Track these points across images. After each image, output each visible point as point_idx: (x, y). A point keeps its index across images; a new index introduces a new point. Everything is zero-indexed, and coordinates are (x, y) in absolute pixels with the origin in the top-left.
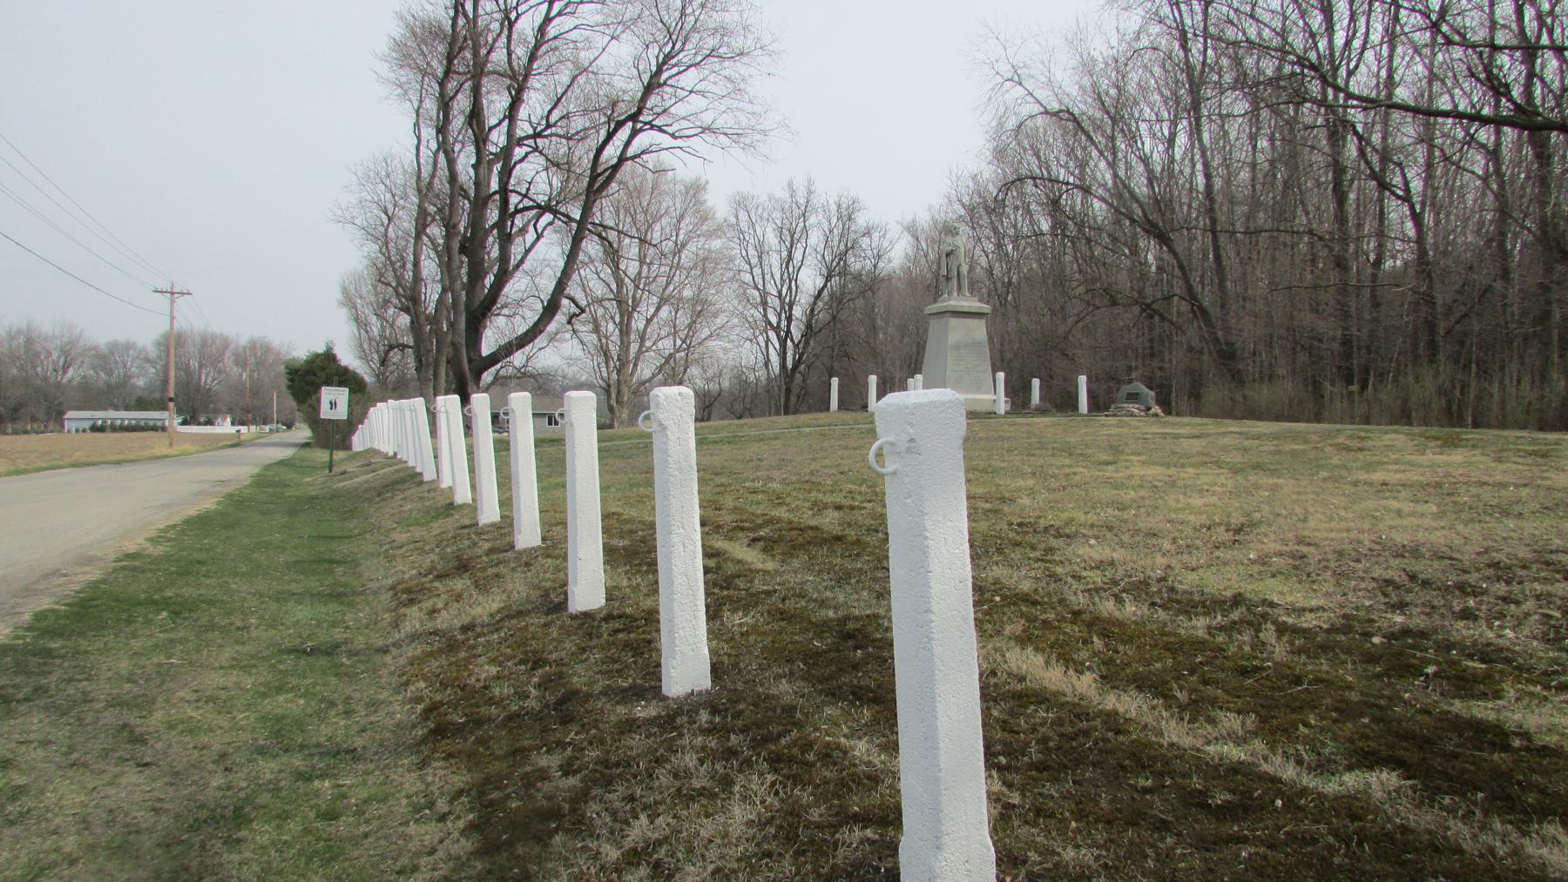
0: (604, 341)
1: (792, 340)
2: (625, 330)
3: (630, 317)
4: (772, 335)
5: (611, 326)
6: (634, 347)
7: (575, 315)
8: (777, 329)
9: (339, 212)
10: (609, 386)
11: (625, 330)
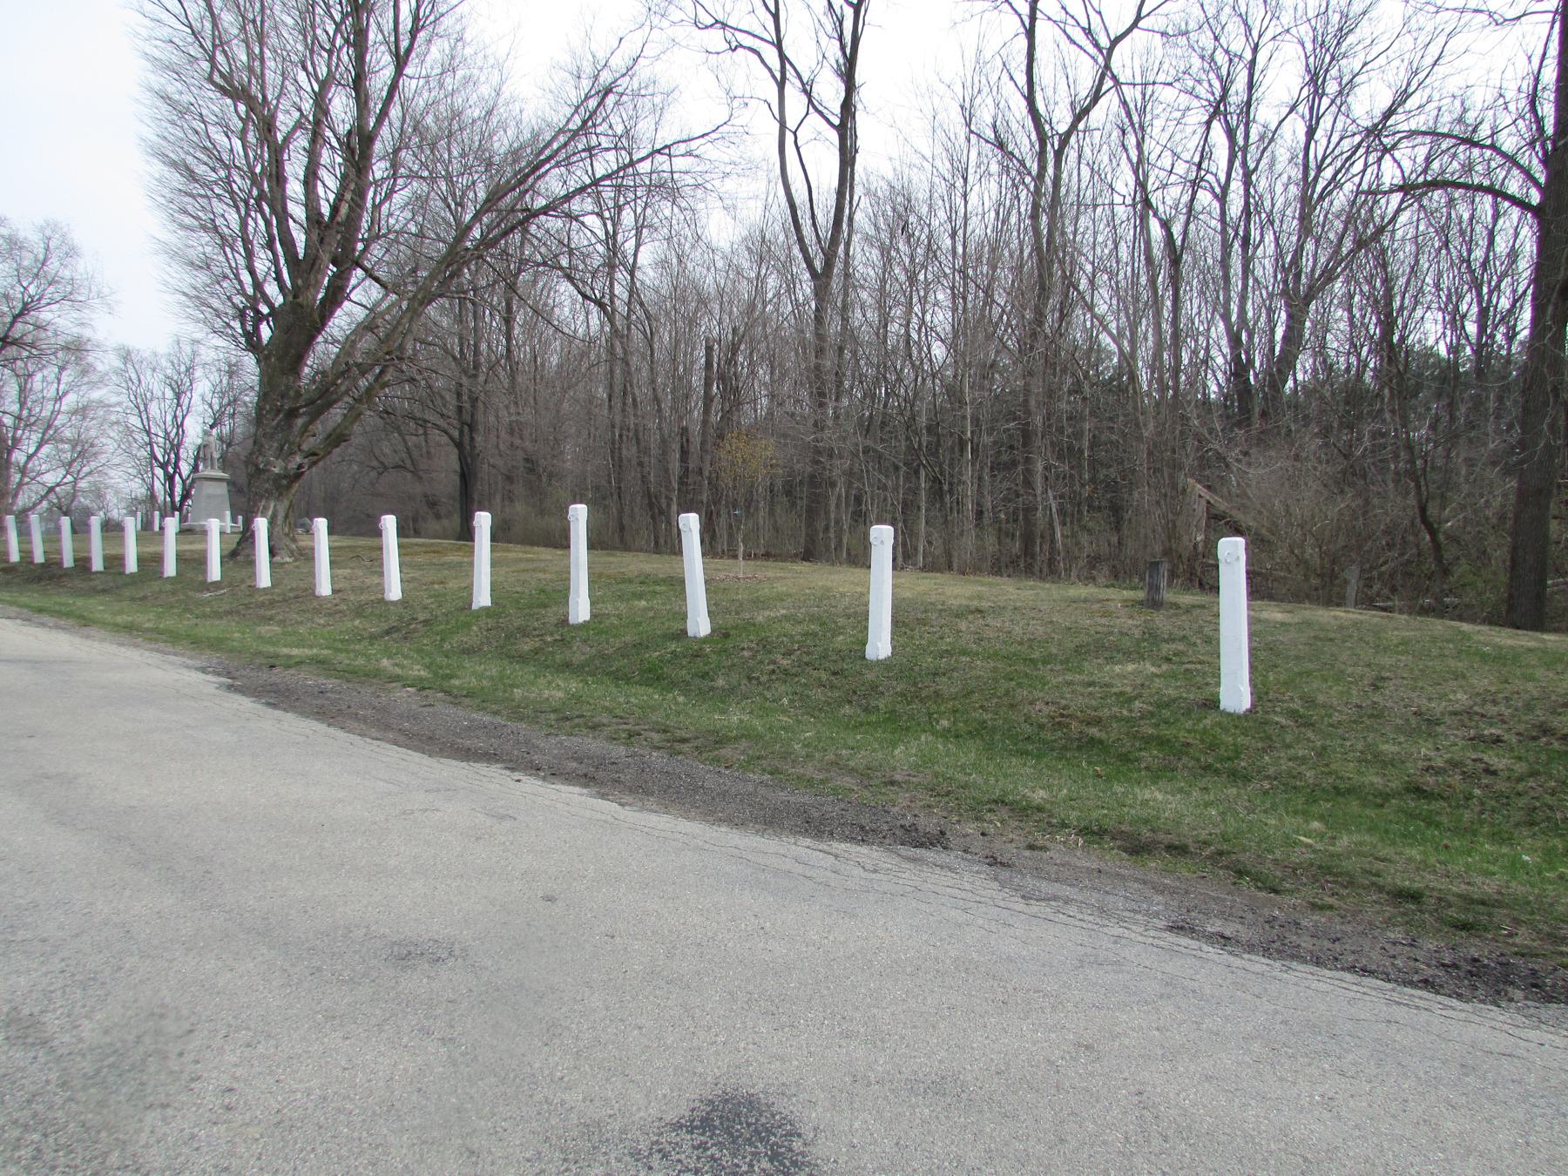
4: (159, 472)
8: (164, 466)
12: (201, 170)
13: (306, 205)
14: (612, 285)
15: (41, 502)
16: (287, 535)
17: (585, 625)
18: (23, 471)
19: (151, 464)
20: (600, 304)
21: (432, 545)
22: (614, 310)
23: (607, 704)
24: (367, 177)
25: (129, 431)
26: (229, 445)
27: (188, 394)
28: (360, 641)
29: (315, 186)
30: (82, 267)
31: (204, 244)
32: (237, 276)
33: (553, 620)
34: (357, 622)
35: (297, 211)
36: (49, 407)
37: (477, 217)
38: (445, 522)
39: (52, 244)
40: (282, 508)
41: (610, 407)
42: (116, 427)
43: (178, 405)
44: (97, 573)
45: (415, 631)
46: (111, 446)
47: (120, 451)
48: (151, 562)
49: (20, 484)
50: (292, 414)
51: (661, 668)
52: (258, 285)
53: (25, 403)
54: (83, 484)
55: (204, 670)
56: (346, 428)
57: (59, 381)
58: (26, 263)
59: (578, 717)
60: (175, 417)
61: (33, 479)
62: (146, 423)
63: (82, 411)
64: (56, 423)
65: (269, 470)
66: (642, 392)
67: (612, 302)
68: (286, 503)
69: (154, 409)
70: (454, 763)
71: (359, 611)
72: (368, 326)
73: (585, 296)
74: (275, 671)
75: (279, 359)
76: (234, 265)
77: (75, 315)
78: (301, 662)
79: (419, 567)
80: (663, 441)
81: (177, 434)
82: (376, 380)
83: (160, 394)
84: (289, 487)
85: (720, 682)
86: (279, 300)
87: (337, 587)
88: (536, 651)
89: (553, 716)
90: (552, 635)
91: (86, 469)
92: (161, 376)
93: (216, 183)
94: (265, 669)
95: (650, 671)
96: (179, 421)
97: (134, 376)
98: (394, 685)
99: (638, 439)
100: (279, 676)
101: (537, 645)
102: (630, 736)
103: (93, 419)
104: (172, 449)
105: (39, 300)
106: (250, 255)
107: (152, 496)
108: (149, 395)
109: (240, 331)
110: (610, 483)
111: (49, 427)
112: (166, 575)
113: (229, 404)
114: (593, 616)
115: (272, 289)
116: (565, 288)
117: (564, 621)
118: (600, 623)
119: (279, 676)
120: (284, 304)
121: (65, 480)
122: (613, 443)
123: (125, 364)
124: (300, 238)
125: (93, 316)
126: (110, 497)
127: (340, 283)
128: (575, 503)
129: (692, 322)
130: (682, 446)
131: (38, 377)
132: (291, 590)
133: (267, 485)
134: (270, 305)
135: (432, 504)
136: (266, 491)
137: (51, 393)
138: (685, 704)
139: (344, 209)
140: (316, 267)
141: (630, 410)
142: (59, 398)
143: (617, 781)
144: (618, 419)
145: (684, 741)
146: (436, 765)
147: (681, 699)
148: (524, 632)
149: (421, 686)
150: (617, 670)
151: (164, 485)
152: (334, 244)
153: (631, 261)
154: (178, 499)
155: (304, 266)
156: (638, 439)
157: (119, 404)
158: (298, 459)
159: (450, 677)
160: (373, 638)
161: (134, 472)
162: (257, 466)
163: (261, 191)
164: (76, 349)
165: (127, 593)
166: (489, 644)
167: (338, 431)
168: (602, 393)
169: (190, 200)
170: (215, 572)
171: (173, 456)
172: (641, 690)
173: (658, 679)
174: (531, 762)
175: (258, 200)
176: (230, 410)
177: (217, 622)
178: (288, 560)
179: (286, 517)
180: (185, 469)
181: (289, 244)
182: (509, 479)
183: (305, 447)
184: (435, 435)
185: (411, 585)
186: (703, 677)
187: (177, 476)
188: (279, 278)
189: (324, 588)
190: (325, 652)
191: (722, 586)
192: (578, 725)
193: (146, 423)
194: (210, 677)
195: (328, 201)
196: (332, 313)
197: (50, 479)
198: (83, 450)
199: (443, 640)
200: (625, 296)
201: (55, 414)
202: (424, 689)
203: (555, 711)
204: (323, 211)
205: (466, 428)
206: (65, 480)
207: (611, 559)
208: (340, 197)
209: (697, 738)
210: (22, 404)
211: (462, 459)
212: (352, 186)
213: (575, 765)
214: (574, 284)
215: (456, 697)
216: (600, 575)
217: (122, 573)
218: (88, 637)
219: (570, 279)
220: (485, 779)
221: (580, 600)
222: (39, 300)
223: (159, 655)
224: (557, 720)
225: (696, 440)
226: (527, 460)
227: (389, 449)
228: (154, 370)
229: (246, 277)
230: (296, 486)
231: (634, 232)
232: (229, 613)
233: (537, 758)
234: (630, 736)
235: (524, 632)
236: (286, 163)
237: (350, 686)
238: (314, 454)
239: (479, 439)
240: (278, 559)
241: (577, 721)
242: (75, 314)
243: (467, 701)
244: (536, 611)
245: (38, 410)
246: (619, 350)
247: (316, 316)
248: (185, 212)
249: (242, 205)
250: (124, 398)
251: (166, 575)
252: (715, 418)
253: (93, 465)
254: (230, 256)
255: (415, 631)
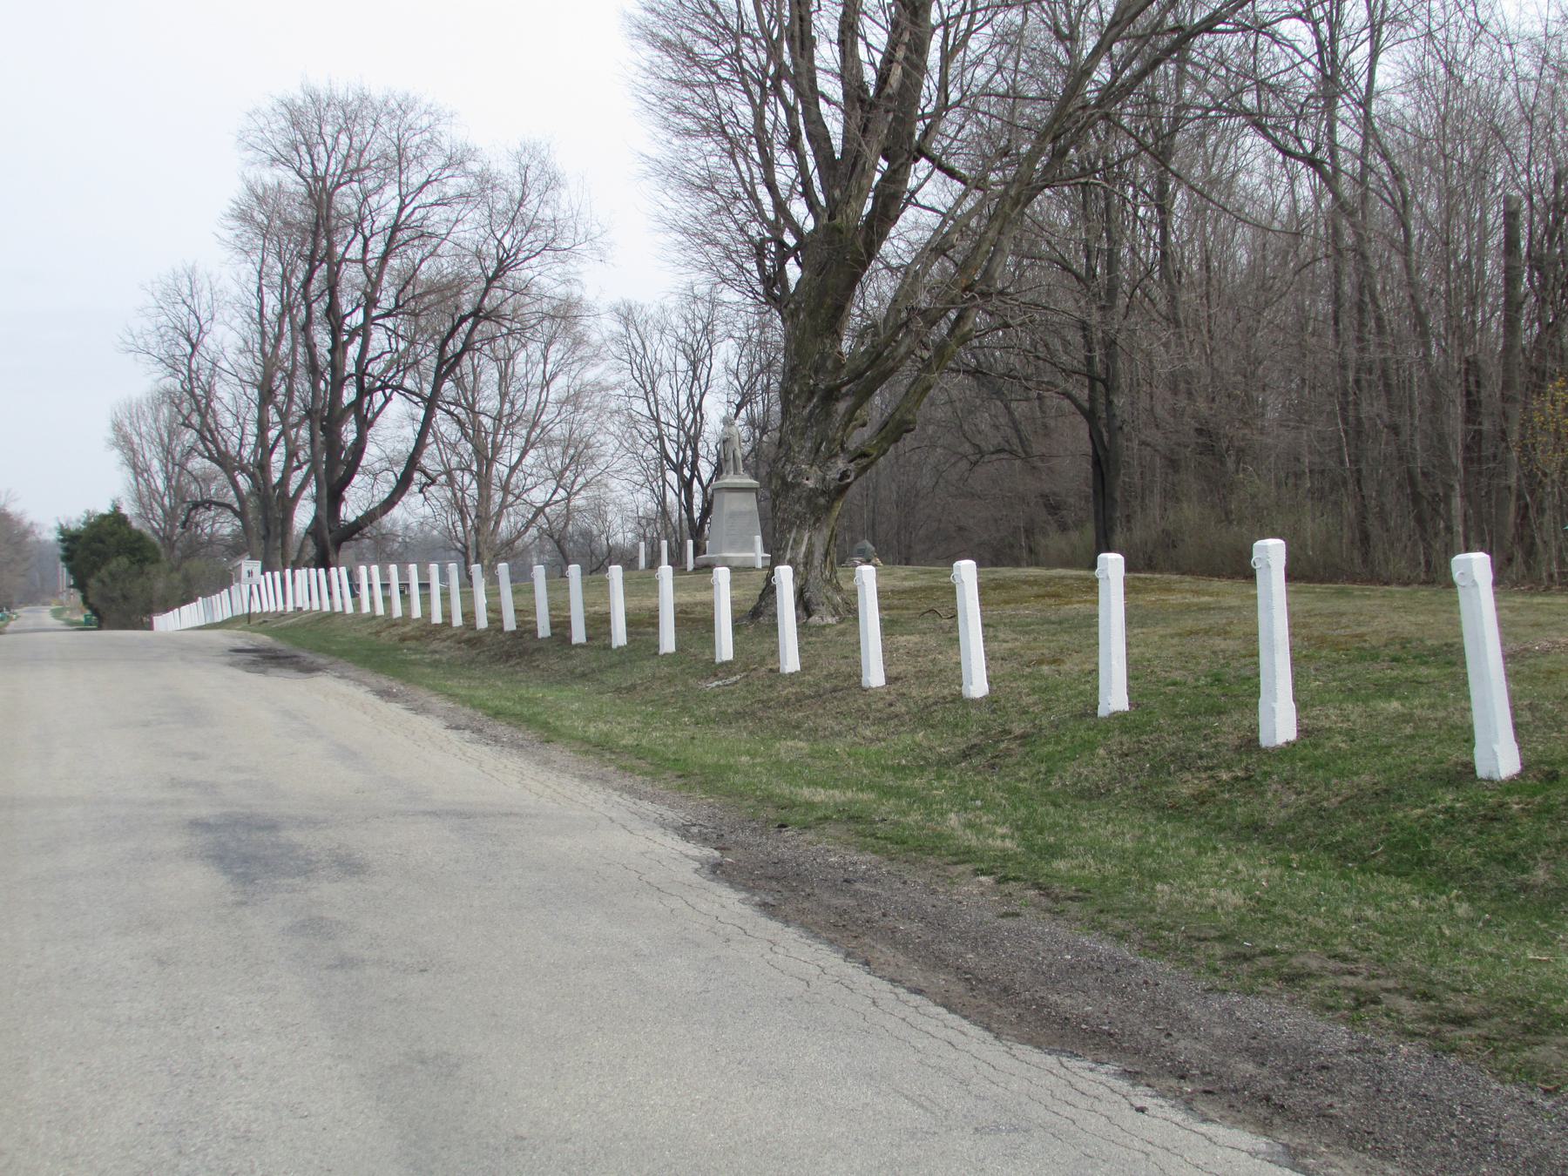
0: (459, 494)
1: (700, 482)
2: (483, 480)
3: (489, 466)
4: (672, 477)
5: (467, 478)
6: (497, 497)
7: (426, 484)
8: (678, 468)
9: (130, 340)
10: (466, 547)
11: (483, 480)
12: (701, 47)
13: (842, 77)
14: (1331, 130)
15: (527, 528)
16: (829, 581)
17: (1288, 750)
18: (505, 488)
19: (662, 466)
20: (1312, 161)
21: (1051, 579)
22: (1336, 169)
23: (1320, 924)
24: (927, 19)
25: (632, 422)
26: (764, 431)
27: (707, 361)
28: (922, 769)
29: (855, 45)
30: (565, 201)
31: (708, 154)
32: (753, 196)
33: (1233, 739)
34: (920, 736)
35: (830, 86)
36: (534, 398)
37: (1102, 48)
38: (1074, 536)
39: (531, 176)
40: (820, 539)
41: (1337, 334)
42: (616, 418)
43: (695, 378)
44: (577, 646)
45: (1008, 753)
46: (611, 445)
47: (622, 452)
48: (643, 623)
49: (503, 505)
50: (831, 396)
51: (1427, 842)
52: (780, 207)
53: (506, 394)
54: (578, 501)
55: (684, 832)
56: (909, 411)
57: (546, 358)
58: (499, 206)
59: (1265, 953)
60: (691, 396)
61: (518, 497)
62: (654, 409)
63: (573, 399)
64: (544, 418)
65: (799, 484)
66: (1391, 300)
67: (1333, 155)
68: (826, 532)
69: (664, 389)
70: (1035, 1056)
71: (923, 717)
72: (937, 248)
73: (1286, 152)
74: (787, 833)
75: (812, 314)
76: (747, 179)
77: (558, 270)
78: (826, 818)
79: (1022, 628)
80: (1434, 387)
81: (694, 419)
82: (951, 331)
83: (671, 366)
84: (828, 508)
85: (1540, 875)
86: (809, 225)
87: (894, 671)
88: (1202, 799)
89: (1219, 950)
90: (1229, 768)
91: (581, 480)
92: (673, 340)
93: (721, 62)
94: (772, 830)
95: (1404, 845)
96: (696, 400)
97: (637, 343)
98: (961, 868)
99: (1387, 386)
100: (793, 845)
101: (1205, 786)
102: (1359, 1004)
103: (588, 409)
104: (688, 442)
105: (515, 254)
106: (768, 164)
107: (664, 512)
108: (656, 368)
109: (756, 274)
110: (1342, 462)
111: (535, 424)
112: (662, 652)
113: (761, 371)
114: (1303, 731)
115: (798, 209)
116: (1252, 141)
117: (1250, 743)
118: (1316, 746)
119: (793, 845)
120: (815, 230)
121: (556, 497)
122: (1345, 394)
123: (627, 329)
124: (834, 125)
125: (581, 268)
126: (614, 519)
127: (892, 188)
128: (1264, 537)
129: (1480, 173)
130: (1468, 394)
131: (522, 356)
132: (829, 676)
133: (797, 507)
134: (797, 231)
135: (1053, 507)
136: (797, 516)
137: (537, 378)
138: (1470, 922)
139: (897, 72)
140: (859, 168)
141: (1372, 338)
142: (546, 383)
143: (1323, 1114)
144: (1352, 353)
145: (1462, 1021)
146: (1005, 1061)
147: (1463, 909)
148: (1183, 761)
149: (1001, 870)
150: (1345, 841)
151: (679, 496)
152: (883, 125)
153: (1362, 83)
154: (697, 514)
155: (842, 169)
156: (1387, 386)
157: (620, 384)
158: (841, 464)
159: (1054, 852)
160: (944, 763)
161: (641, 479)
162: (783, 479)
163: (781, 66)
164: (565, 315)
165: (611, 678)
166: (1124, 781)
167: (897, 416)
168: (1324, 307)
169: (686, 93)
170: (725, 648)
171: (689, 453)
172: (1388, 885)
173: (1420, 863)
174: (1171, 1056)
175: (777, 78)
176: (763, 379)
177: (723, 732)
178: (830, 620)
179: (827, 554)
180: (706, 470)
181: (820, 137)
182: (1173, 464)
183: (852, 445)
184: (1053, 400)
185: (1008, 667)
186: (1505, 862)
187: (696, 482)
188: (808, 194)
189: (875, 676)
190: (864, 796)
191: (1545, 663)
192: (1263, 972)
193: (654, 409)
194: (693, 849)
195: (873, 64)
196: (883, 236)
197: (538, 496)
198: (578, 453)
199: (1049, 771)
200: (1356, 142)
201: (541, 408)
202: (1005, 880)
203: (1222, 939)
204: (866, 79)
205: (1099, 386)
206: (556, 497)
207: (1343, 604)
208: (889, 59)
209: (1488, 1016)
210: (503, 396)
211: (1095, 436)
212: (906, 37)
213: (1250, 1068)
214: (1267, 136)
215: (1056, 900)
216: (1322, 641)
217: (608, 647)
218: (546, 762)
219: (1261, 128)
220: (1083, 1103)
221: (1278, 706)
222: (515, 254)
223: (627, 800)
224: (1226, 959)
225: (1493, 372)
226: (1199, 431)
227: (987, 422)
228: (662, 332)
229: (763, 193)
230: (839, 506)
231: (1365, 34)
232: (740, 715)
233: (1185, 1047)
234: (1359, 1004)
235: (1183, 761)
236: (814, 16)
237: (893, 869)
238: (864, 455)
239: (1120, 401)
240: (815, 619)
241: (1263, 962)
242: (558, 269)
243: (1074, 908)
244: (1203, 720)
245: (521, 401)
246: (1348, 239)
247: (860, 242)
248: (679, 110)
249: (756, 89)
250: (626, 375)
251: (662, 652)
252: (1529, 332)
253: (590, 473)
254: (743, 167)
255: (1008, 753)
